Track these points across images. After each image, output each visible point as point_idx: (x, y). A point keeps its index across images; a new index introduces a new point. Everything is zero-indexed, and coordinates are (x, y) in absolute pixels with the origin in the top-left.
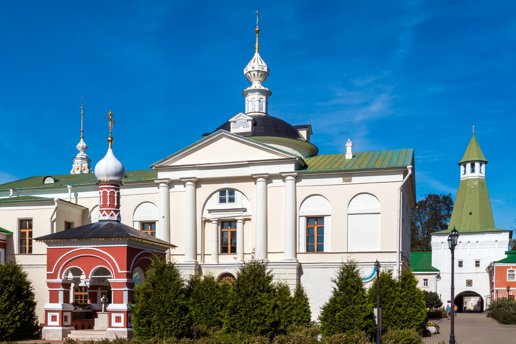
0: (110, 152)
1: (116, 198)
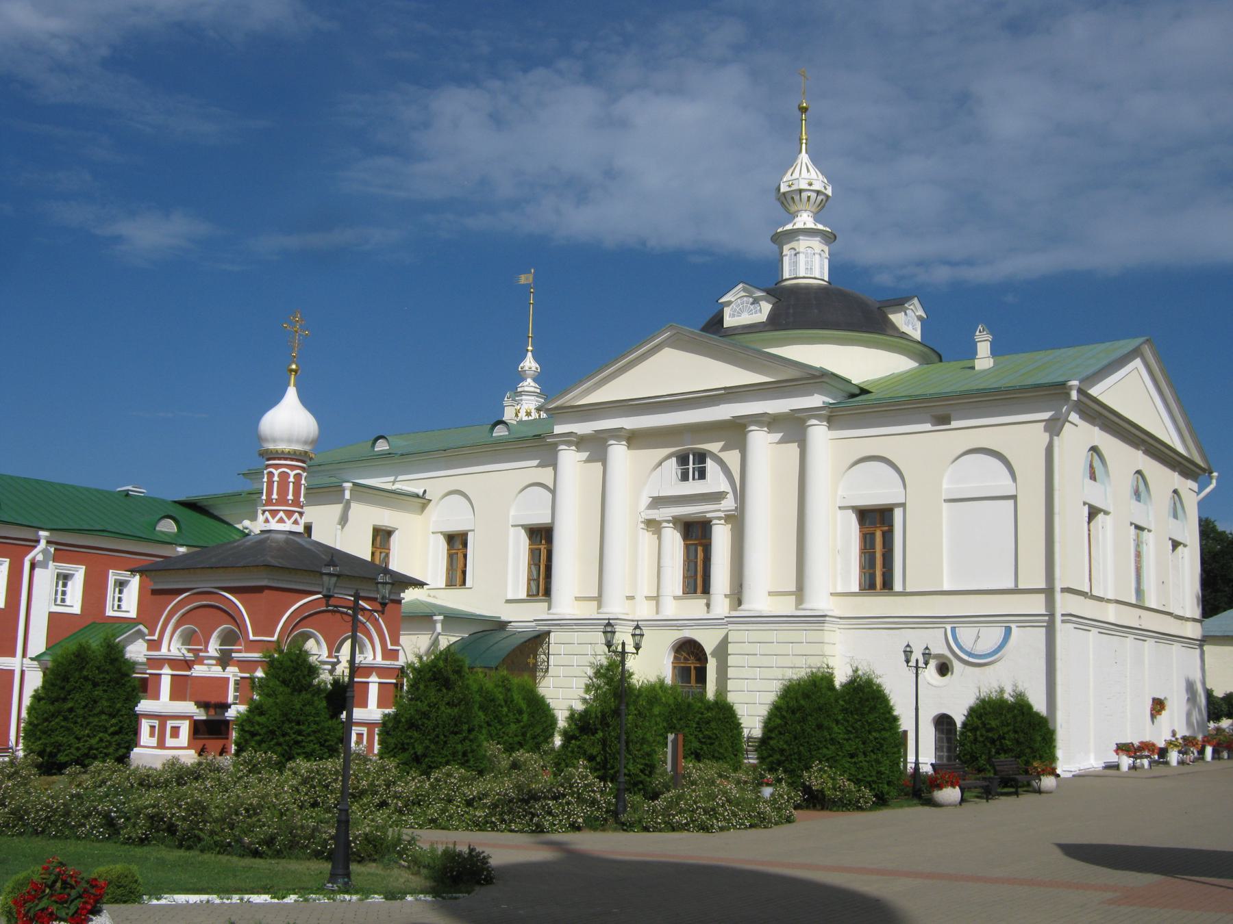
0: (291, 394)
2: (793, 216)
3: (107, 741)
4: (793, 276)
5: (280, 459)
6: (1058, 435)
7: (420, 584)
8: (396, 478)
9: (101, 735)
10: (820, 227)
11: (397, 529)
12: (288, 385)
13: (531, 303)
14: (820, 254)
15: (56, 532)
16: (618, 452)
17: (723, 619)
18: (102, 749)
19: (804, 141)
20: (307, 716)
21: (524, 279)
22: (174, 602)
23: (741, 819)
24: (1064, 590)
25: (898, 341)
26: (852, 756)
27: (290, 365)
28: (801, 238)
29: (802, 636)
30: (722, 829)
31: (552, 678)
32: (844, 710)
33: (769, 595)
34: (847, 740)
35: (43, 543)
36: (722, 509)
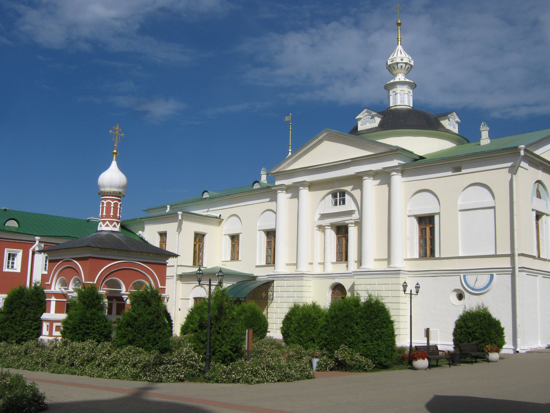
0: (114, 164)
1: (119, 209)
2: (395, 76)
3: (32, 333)
4: (394, 105)
5: (107, 196)
6: (515, 174)
7: (176, 256)
8: (208, 210)
9: (28, 330)
10: (407, 80)
11: (207, 233)
12: (113, 160)
13: (290, 130)
14: (408, 94)
15: (43, 237)
16: (304, 192)
17: (352, 273)
18: (29, 337)
19: (399, 39)
20: (93, 320)
21: (287, 119)
22: (56, 266)
23: (273, 377)
24: (520, 255)
25: (446, 134)
26: (364, 342)
27: (114, 150)
28: (398, 86)
29: (390, 281)
30: (258, 382)
31: (275, 303)
32: (361, 317)
33: (375, 261)
34: (362, 333)
35: (37, 242)
36: (353, 219)
